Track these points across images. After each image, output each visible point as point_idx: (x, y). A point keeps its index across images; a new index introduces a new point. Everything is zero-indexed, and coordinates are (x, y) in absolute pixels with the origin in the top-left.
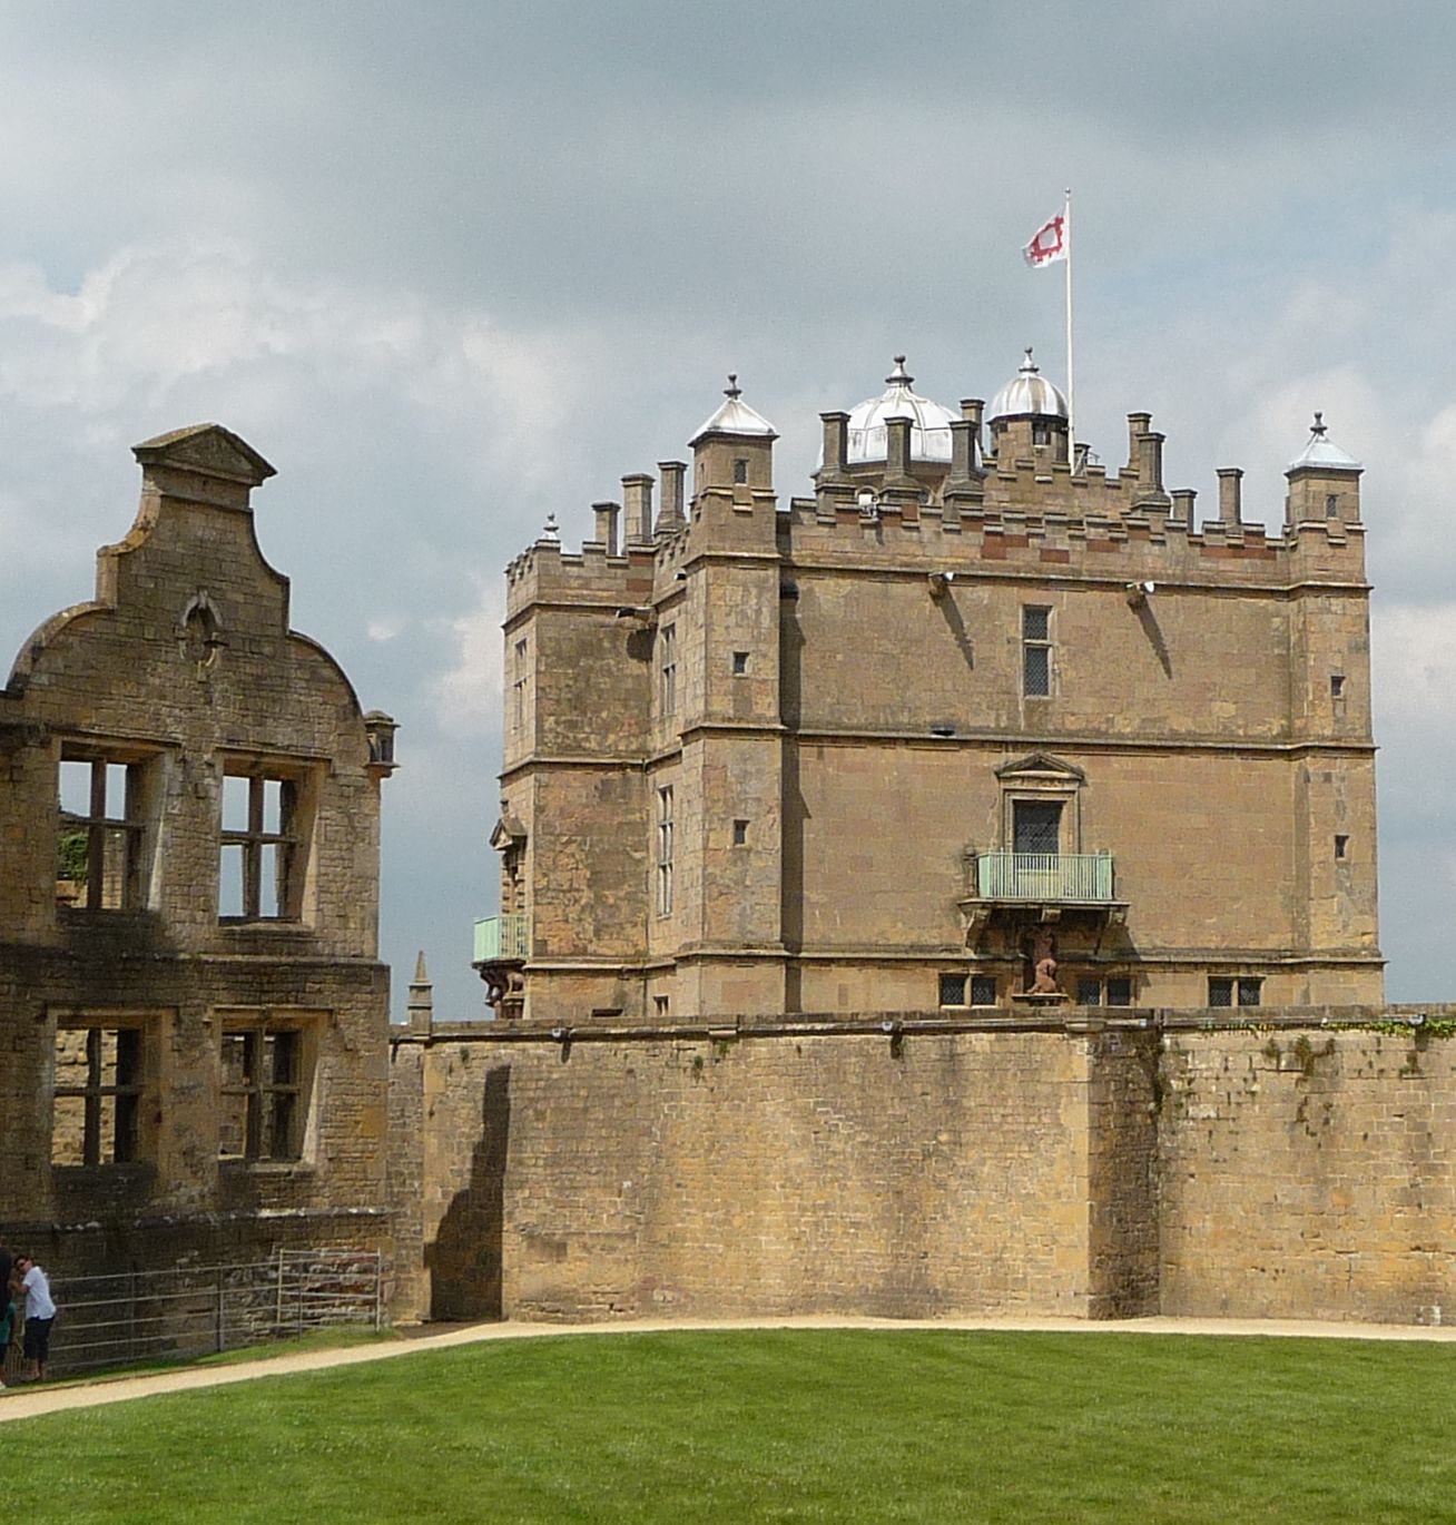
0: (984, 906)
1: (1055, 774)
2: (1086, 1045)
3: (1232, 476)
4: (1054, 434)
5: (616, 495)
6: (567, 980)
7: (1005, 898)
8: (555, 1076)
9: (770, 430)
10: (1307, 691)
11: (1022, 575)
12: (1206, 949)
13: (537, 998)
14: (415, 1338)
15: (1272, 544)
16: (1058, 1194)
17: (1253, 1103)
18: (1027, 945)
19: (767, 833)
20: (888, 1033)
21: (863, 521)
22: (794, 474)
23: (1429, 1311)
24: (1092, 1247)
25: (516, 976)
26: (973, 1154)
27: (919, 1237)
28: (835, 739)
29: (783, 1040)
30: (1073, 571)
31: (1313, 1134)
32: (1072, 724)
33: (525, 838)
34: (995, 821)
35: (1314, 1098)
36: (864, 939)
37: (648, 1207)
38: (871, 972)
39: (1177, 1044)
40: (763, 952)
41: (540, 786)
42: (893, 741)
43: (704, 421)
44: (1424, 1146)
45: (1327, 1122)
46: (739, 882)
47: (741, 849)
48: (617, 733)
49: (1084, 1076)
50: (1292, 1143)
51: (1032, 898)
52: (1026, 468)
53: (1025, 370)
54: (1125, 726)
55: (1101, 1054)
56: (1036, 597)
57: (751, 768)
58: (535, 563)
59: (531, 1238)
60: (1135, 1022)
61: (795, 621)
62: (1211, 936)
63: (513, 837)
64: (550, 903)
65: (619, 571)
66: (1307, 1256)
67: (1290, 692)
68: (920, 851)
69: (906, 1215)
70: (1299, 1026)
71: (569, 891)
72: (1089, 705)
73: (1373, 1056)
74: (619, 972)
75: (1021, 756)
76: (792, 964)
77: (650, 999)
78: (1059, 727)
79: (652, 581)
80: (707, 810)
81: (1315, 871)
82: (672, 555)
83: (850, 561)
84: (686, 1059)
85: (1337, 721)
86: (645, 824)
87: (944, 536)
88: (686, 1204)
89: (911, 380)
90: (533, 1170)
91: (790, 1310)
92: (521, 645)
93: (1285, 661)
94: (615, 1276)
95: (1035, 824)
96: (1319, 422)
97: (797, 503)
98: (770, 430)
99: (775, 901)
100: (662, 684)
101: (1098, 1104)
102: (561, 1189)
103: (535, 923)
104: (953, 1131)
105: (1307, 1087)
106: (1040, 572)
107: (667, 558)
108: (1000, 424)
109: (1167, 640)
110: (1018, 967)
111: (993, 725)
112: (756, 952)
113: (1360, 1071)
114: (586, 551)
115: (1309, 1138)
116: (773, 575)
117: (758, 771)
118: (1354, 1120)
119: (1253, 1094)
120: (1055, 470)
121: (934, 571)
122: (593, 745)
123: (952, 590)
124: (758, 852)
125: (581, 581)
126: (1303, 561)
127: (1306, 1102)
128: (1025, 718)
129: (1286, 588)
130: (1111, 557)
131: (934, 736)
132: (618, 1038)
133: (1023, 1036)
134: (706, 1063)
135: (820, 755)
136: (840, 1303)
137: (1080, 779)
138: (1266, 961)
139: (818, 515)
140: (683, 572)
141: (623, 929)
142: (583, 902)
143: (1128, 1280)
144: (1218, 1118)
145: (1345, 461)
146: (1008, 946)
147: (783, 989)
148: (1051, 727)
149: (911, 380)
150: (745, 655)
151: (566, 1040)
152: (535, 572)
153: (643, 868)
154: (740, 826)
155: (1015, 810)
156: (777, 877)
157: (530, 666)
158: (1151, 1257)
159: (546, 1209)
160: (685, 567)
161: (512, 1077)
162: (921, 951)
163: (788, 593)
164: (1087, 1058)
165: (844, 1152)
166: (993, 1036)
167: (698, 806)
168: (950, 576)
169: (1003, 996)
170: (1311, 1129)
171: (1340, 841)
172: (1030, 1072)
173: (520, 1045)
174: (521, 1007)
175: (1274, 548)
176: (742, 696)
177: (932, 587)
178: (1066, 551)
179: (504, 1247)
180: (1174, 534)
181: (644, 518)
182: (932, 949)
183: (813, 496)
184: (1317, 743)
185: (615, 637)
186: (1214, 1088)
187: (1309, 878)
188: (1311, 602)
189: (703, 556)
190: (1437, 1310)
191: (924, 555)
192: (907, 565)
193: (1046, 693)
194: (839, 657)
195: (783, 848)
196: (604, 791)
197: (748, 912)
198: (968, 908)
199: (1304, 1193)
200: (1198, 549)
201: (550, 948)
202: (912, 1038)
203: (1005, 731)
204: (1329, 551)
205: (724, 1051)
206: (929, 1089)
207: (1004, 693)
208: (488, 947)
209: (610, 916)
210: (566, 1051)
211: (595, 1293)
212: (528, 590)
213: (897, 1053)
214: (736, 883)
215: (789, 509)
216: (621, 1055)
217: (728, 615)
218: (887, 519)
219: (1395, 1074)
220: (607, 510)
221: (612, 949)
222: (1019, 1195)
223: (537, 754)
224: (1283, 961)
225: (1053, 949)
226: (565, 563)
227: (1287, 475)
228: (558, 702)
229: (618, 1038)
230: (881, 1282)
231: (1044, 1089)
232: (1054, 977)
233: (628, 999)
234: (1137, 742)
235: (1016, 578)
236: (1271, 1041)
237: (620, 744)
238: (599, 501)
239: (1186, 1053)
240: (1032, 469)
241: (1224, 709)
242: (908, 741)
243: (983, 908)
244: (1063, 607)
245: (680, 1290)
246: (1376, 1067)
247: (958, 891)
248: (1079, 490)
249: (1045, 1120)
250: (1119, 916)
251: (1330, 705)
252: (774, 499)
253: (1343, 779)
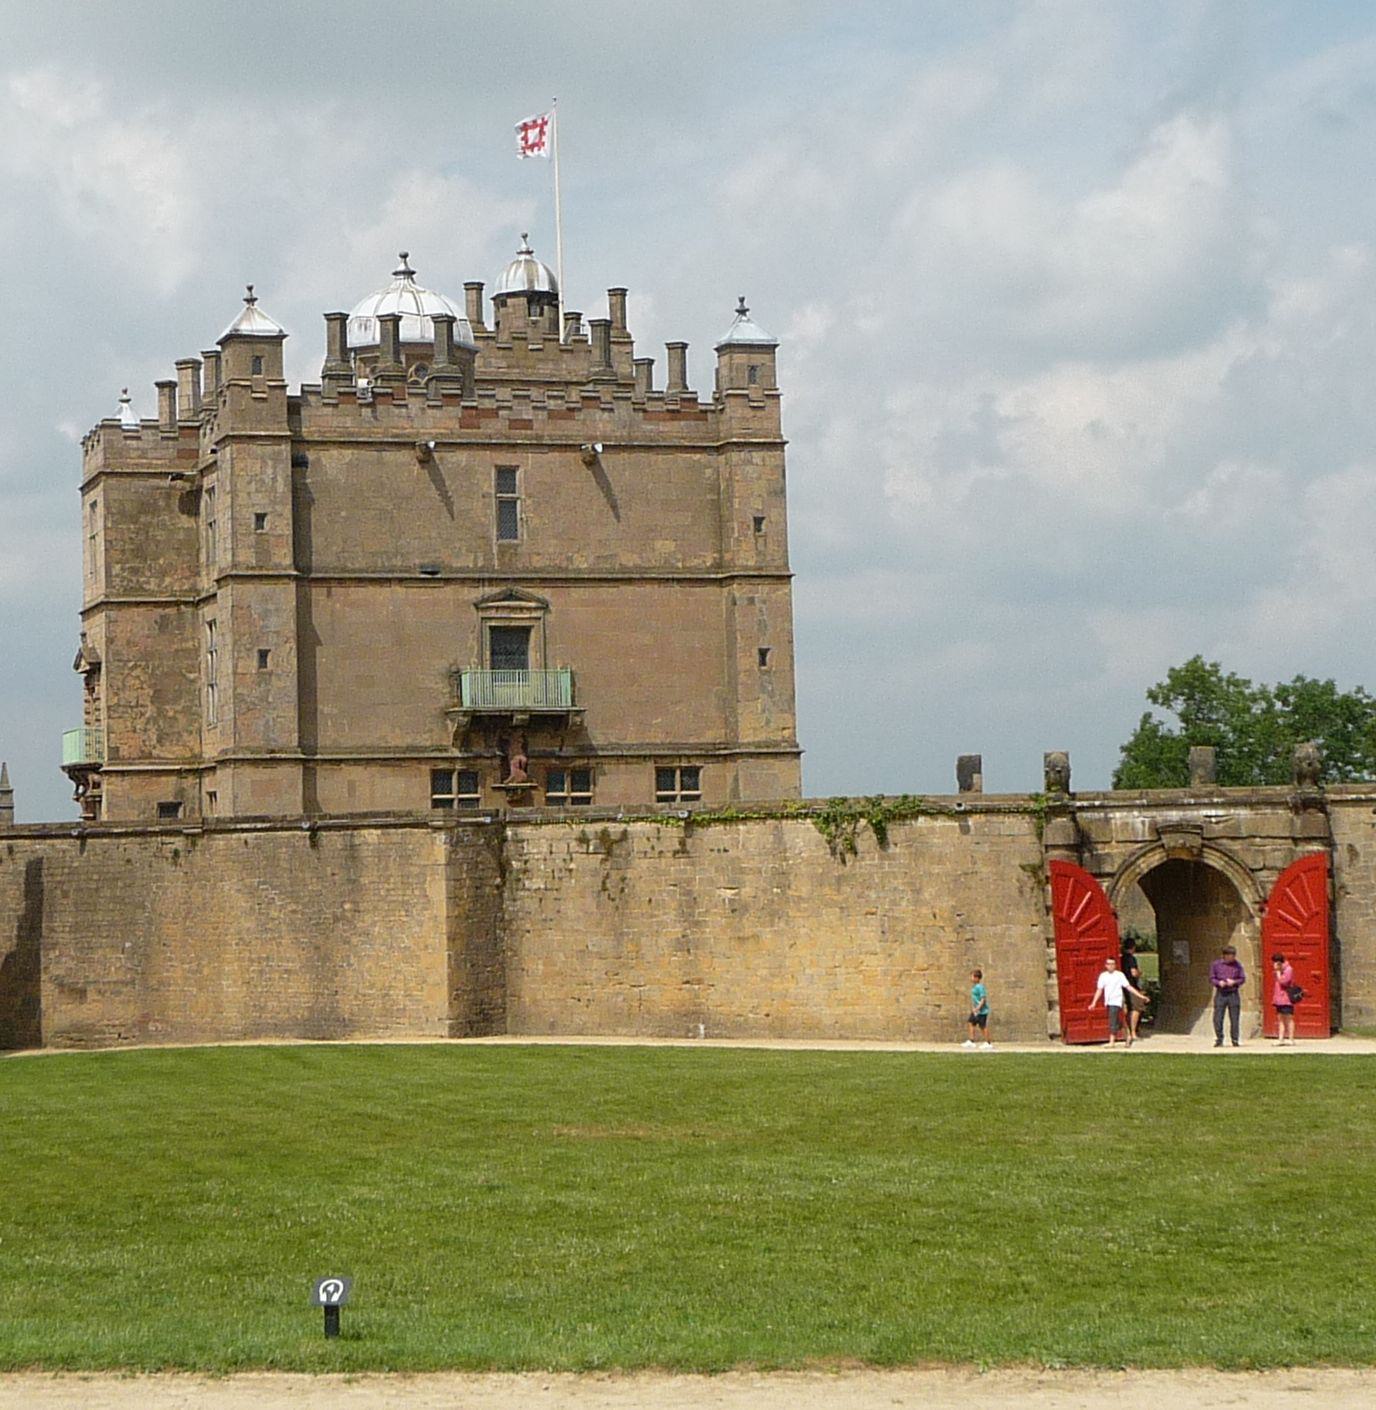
0: (465, 713)
1: (523, 604)
2: (444, 837)
3: (678, 349)
4: (546, 307)
5: (172, 376)
6: (136, 780)
7: (481, 706)
8: (76, 864)
9: (281, 331)
10: (733, 529)
11: (494, 441)
12: (652, 744)
13: (110, 793)
14: (1114, 1360)
15: (704, 408)
16: (426, 947)
17: (571, 878)
18: (504, 744)
19: (285, 658)
20: (308, 830)
21: (360, 401)
22: (304, 366)
23: (697, 1027)
24: (451, 986)
25: (93, 777)
26: (368, 918)
27: (332, 981)
28: (341, 581)
29: (235, 836)
30: (538, 437)
31: (613, 900)
32: (537, 562)
33: (100, 664)
34: (475, 643)
35: (613, 873)
36: (368, 742)
37: (143, 958)
38: (374, 769)
39: (516, 834)
40: (283, 756)
41: (110, 622)
42: (389, 580)
43: (226, 327)
44: (690, 907)
45: (622, 890)
46: (264, 699)
47: (264, 674)
48: (172, 576)
49: (443, 861)
50: (598, 907)
51: (505, 706)
52: (518, 339)
53: (521, 253)
54: (582, 563)
55: (455, 844)
56: (505, 459)
57: (271, 607)
58: (102, 438)
59: (61, 985)
60: (481, 819)
61: (305, 484)
62: (657, 734)
63: (90, 664)
64: (120, 717)
65: (171, 443)
66: (609, 990)
67: (720, 530)
68: (415, 665)
69: (323, 964)
70: (602, 820)
71: (137, 706)
72: (552, 546)
73: (654, 841)
74: (179, 772)
75: (495, 590)
76: (309, 764)
77: (204, 793)
78: (527, 565)
79: (198, 451)
80: (235, 643)
81: (742, 677)
82: (212, 429)
83: (351, 434)
84: (168, 850)
85: (759, 553)
86: (197, 650)
87: (430, 412)
88: (170, 959)
89: (413, 273)
90: (61, 935)
91: (245, 1035)
92: (94, 505)
93: (717, 505)
94: (122, 1012)
95: (508, 647)
96: (742, 305)
97: (306, 388)
98: (281, 331)
99: (292, 713)
100: (207, 535)
101: (455, 881)
102: (81, 949)
103: (108, 733)
104: (354, 902)
105: (608, 865)
106: (508, 437)
107: (208, 431)
108: (501, 300)
109: (616, 490)
110: (497, 762)
111: (471, 566)
112: (278, 755)
113: (646, 853)
114: (143, 427)
115: (611, 903)
116: (285, 449)
117: (277, 610)
118: (642, 889)
119: (571, 870)
120: (545, 340)
121: (420, 441)
122: (152, 586)
123: (436, 455)
124: (278, 675)
125: (140, 452)
126: (729, 423)
127: (607, 876)
128: (499, 559)
129: (715, 444)
130: (571, 423)
131: (423, 576)
132: (119, 835)
133: (400, 831)
134: (182, 854)
135: (329, 594)
136: (278, 1029)
137: (544, 606)
138: (703, 752)
139: (323, 398)
140: (214, 447)
141: (181, 736)
142: (147, 715)
143: (482, 1004)
144: (546, 889)
145: (762, 337)
146: (488, 747)
147: (301, 787)
148: (520, 566)
149: (413, 273)
150: (265, 515)
151: (82, 837)
152: (102, 446)
153: (198, 686)
154: (263, 655)
155: (491, 634)
156: (294, 694)
157: (100, 524)
158: (500, 991)
159: (71, 964)
160: (217, 443)
161: (45, 866)
162: (419, 752)
163: (299, 463)
164: (444, 847)
165: (279, 917)
166: (379, 832)
167: (229, 639)
168: (432, 444)
169: (484, 787)
170: (612, 896)
171: (763, 653)
172: (405, 858)
173: (48, 841)
174: (100, 802)
175: (706, 412)
176: (262, 550)
177: (419, 454)
178: (530, 421)
179: (43, 993)
180: (621, 402)
181: (194, 395)
182: (425, 749)
183: (320, 382)
184: (742, 573)
185: (168, 496)
186: (542, 867)
187: (737, 684)
188: (735, 456)
189: (227, 436)
190: (702, 1027)
191: (412, 427)
192: (397, 436)
193: (516, 538)
194: (343, 514)
195: (299, 672)
196: (163, 624)
197: (271, 723)
198: (453, 716)
199: (607, 944)
200: (641, 414)
201: (121, 754)
202: (324, 833)
204: (750, 413)
205: (194, 844)
206: (336, 871)
208: (74, 756)
209: (171, 726)
210: (83, 845)
211: (108, 1026)
212: (97, 461)
213: (314, 844)
214: (261, 700)
215: (299, 394)
216: (121, 849)
217: (249, 483)
218: (380, 398)
219: (670, 855)
220: (167, 387)
221: (173, 753)
222: (400, 948)
223: (106, 596)
224: (717, 753)
225: (525, 748)
226: (126, 438)
227: (716, 349)
228: (123, 551)
229: (119, 835)
230: (306, 1014)
231: (415, 870)
232: (526, 771)
233: (185, 793)
234: (592, 576)
235: (488, 444)
236: (583, 832)
237: (176, 584)
238: (160, 380)
239: (523, 841)
240: (525, 339)
241: (665, 546)
242: (401, 580)
243: (464, 716)
244: (528, 466)
245: (167, 1022)
246: (657, 850)
247: (444, 701)
248: (565, 355)
249: (417, 892)
250: (578, 719)
251: (753, 540)
252: (286, 386)
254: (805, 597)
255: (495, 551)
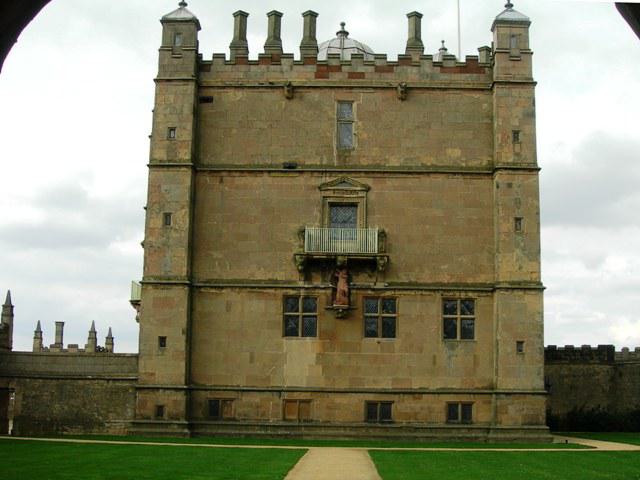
32: (364, 162)
54: (394, 162)
72: (375, 152)
135: (221, 181)
146: (324, 281)
176: (171, 150)
194: (234, 131)
203: (326, 166)
204: (511, 64)
207: (325, 146)
242: (366, 172)
253: (519, 186)
254: (549, 301)
255: (335, 155)
